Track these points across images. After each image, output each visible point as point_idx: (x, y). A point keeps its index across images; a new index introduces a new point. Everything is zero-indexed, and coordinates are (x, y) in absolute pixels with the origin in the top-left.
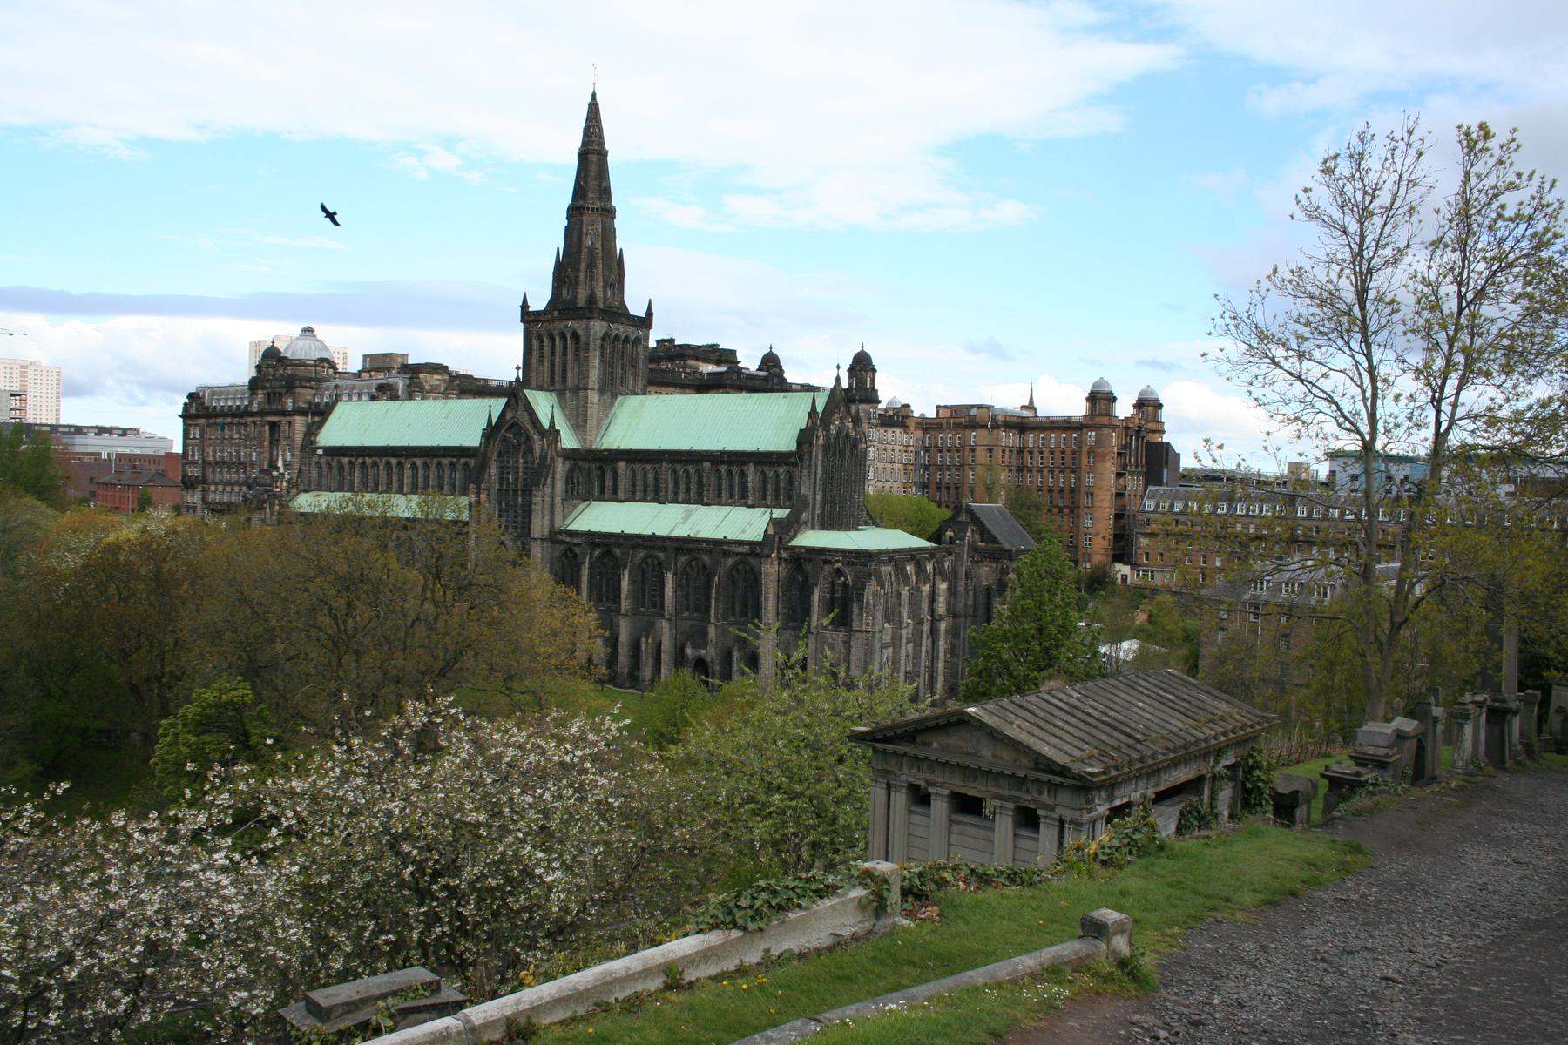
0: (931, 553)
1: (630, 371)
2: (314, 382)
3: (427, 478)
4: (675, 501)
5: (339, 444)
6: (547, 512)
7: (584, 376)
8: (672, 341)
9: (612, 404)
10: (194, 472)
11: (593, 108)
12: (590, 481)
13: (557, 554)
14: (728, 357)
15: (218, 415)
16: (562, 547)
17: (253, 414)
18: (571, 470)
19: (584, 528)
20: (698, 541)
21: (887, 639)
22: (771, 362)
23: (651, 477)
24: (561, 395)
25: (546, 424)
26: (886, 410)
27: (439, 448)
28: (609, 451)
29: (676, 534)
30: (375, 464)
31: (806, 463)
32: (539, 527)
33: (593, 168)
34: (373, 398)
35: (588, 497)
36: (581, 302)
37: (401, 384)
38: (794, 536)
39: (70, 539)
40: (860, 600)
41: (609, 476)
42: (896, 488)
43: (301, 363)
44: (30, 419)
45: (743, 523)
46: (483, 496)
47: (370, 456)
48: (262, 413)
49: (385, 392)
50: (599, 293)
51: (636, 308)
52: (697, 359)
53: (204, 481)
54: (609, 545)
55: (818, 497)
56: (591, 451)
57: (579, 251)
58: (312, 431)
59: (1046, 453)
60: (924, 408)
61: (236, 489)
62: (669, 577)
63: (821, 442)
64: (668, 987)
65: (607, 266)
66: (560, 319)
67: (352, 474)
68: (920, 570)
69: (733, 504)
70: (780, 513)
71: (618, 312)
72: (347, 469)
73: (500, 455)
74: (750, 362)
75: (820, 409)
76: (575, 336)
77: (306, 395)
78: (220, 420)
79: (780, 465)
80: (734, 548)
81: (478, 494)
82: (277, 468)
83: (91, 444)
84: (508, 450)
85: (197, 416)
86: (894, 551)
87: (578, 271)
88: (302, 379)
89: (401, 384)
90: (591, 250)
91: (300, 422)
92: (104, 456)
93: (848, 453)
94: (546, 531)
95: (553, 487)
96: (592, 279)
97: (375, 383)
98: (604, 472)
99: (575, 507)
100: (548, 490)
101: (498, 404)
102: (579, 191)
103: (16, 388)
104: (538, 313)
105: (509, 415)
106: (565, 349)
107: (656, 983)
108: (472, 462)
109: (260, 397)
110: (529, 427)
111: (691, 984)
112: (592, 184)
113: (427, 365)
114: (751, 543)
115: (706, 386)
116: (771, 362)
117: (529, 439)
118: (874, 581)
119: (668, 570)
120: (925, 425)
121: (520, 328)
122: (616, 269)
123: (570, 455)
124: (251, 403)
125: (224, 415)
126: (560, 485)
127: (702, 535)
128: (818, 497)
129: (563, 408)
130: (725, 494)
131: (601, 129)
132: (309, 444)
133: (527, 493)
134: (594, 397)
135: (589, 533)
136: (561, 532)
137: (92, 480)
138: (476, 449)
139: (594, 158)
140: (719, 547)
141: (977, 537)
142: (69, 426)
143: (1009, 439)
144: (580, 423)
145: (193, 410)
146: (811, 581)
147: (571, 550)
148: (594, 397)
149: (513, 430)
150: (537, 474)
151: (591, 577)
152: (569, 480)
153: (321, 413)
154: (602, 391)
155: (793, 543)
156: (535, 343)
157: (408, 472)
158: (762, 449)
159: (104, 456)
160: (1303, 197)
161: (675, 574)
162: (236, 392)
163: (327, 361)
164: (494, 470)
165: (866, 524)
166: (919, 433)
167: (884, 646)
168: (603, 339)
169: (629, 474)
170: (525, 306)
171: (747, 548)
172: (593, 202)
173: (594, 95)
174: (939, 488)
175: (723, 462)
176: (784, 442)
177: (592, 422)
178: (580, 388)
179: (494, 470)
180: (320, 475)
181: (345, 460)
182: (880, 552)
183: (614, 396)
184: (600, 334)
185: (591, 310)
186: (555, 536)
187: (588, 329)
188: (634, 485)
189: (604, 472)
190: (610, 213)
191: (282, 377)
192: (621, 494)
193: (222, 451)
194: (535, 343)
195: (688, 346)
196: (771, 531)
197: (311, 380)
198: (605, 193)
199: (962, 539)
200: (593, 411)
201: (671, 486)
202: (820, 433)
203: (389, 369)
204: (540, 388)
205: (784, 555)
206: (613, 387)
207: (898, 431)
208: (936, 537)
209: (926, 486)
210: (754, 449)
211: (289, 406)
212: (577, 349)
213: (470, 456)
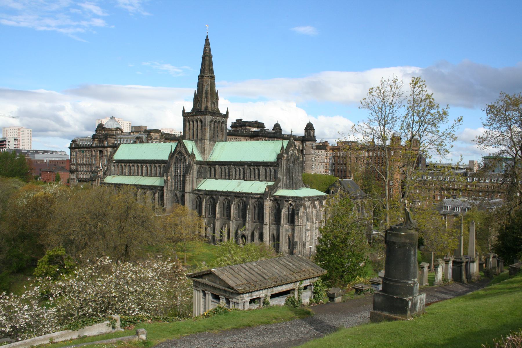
0: (325, 198)
1: (220, 132)
2: (114, 136)
3: (151, 171)
4: (235, 179)
5: (121, 159)
6: (191, 183)
7: (203, 135)
8: (241, 120)
9: (214, 145)
10: (73, 167)
12: (206, 172)
13: (194, 198)
14: (261, 125)
15: (82, 148)
16: (196, 195)
17: (93, 147)
18: (200, 168)
19: (204, 189)
20: (242, 193)
21: (308, 228)
22: (277, 127)
23: (227, 170)
24: (196, 141)
25: (190, 152)
26: (319, 144)
27: (155, 160)
28: (213, 161)
29: (235, 191)
30: (133, 166)
31: (280, 166)
32: (188, 188)
33: (207, 62)
34: (135, 142)
35: (205, 178)
36: (203, 109)
37: (144, 137)
38: (276, 192)
39: (24, 193)
40: (298, 215)
41: (213, 170)
42: (323, 172)
43: (110, 129)
44: (21, 148)
45: (257, 187)
46: (169, 178)
47: (131, 163)
48: (97, 147)
49: (139, 140)
50: (209, 105)
51: (223, 111)
52: (250, 126)
53: (77, 171)
54: (213, 195)
55: (284, 178)
56: (206, 162)
57: (202, 91)
58: (112, 154)
60: (333, 142)
61: (88, 173)
62: (232, 206)
63: (285, 158)
64: (51, 343)
65: (212, 96)
66: (196, 115)
67: (125, 169)
68: (321, 203)
69: (255, 180)
70: (270, 183)
71: (216, 113)
72: (124, 167)
73: (175, 163)
74: (269, 127)
75: (285, 147)
76: (201, 121)
77: (112, 141)
78: (83, 149)
79: (271, 166)
80: (255, 196)
81: (167, 177)
82: (100, 168)
83: (38, 157)
84: (178, 161)
85: (75, 148)
86: (310, 197)
87: (202, 98)
88: (110, 135)
89: (144, 137)
90: (206, 91)
91: (110, 150)
92: (45, 161)
93: (295, 162)
94: (191, 190)
95: (193, 174)
96: (207, 101)
97: (135, 136)
98: (211, 168)
99: (201, 181)
100: (191, 175)
101: (173, 145)
102: (202, 70)
103: (16, 137)
104: (188, 113)
105: (178, 149)
106: (198, 125)
107: (48, 342)
108: (166, 165)
109: (96, 141)
110: (185, 153)
111: (57, 342)
112: (207, 68)
113: (153, 130)
114: (260, 194)
115: (254, 136)
116: (277, 127)
117: (185, 158)
118: (303, 207)
119: (232, 203)
120: (333, 149)
121: (182, 118)
122: (215, 97)
123: (200, 163)
124: (93, 143)
125: (84, 148)
126: (195, 174)
127: (244, 191)
128: (284, 178)
129: (197, 146)
130: (253, 177)
131: (210, 48)
132: (110, 159)
133: (184, 176)
134: (207, 142)
135: (205, 191)
136: (196, 190)
137: (40, 169)
138: (167, 161)
139: (207, 58)
140: (249, 195)
141: (342, 191)
142: (33, 150)
143: (364, 154)
144: (203, 152)
145: (73, 146)
146: (281, 207)
147: (199, 197)
148: (207, 142)
149: (179, 155)
150: (188, 169)
151: (206, 206)
152: (199, 172)
153: (115, 147)
154: (210, 140)
155: (275, 194)
156: (187, 124)
157: (144, 169)
158: (265, 161)
159: (45, 161)
160: (363, 101)
161: (235, 205)
162: (88, 140)
163: (119, 128)
164: (173, 168)
165: (303, 187)
166: (331, 152)
167: (307, 230)
168: (211, 122)
169: (220, 170)
170: (184, 111)
171: (259, 196)
172: (207, 73)
173: (207, 36)
174: (338, 171)
175: (252, 166)
176: (271, 158)
177: (207, 152)
178: (203, 139)
179: (173, 168)
180: (114, 170)
181: (123, 164)
182: (305, 197)
183: (215, 142)
184: (209, 120)
185: (206, 112)
186: (194, 192)
187: (205, 119)
188: (221, 173)
189: (211, 168)
190: (213, 78)
191: (104, 135)
192: (217, 177)
193: (83, 160)
194: (187, 124)
195: (247, 122)
196: (267, 190)
197: (113, 135)
198: (212, 71)
199: (336, 192)
200: (207, 147)
201: (234, 173)
202: (285, 155)
203: (140, 131)
204: (189, 139)
205: (272, 198)
206: (214, 139)
207: (323, 151)
208: (328, 192)
209: (334, 171)
210: (262, 161)
211: (106, 144)
212: (202, 126)
213: (165, 163)
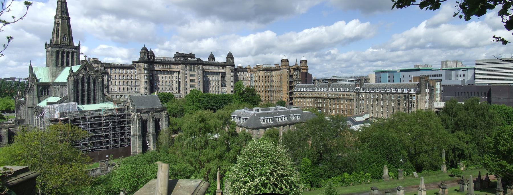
51: (76, 44)
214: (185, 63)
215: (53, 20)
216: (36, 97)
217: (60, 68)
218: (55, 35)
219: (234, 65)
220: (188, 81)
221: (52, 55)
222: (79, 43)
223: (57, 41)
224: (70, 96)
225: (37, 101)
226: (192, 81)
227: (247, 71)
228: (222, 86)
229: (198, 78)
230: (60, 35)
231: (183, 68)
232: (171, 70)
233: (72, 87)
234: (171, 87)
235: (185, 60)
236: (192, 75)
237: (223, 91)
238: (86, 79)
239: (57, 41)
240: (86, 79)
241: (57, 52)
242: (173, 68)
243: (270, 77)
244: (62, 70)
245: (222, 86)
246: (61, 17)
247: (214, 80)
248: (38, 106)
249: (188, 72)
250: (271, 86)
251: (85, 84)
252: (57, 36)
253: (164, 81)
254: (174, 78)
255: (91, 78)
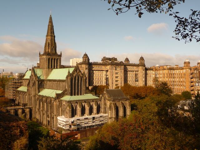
11: (51, 18)
51: (59, 53)
59: (177, 74)
170: (40, 54)
173: (51, 16)
183: (52, 69)
207: (151, 71)
214: (112, 64)
215: (139, 61)
216: (37, 89)
217: (50, 70)
218: (47, 47)
219: (145, 66)
220: (114, 77)
221: (46, 61)
222: (61, 53)
223: (48, 51)
224: (68, 89)
225: (38, 92)
226: (117, 77)
227: (152, 70)
228: (136, 81)
229: (121, 74)
230: (50, 48)
231: (111, 68)
232: (132, 70)
233: (70, 84)
234: (101, 81)
235: (112, 62)
236: (117, 73)
237: (136, 84)
238: (77, 78)
239: (48, 51)
240: (77, 78)
241: (49, 59)
242: (103, 68)
243: (172, 75)
244: (51, 71)
245: (136, 81)
246: (51, 36)
247: (131, 76)
248: (43, 96)
249: (114, 71)
250: (174, 81)
251: (77, 81)
252: (49, 48)
253: (97, 78)
254: (104, 75)
255: (79, 77)
